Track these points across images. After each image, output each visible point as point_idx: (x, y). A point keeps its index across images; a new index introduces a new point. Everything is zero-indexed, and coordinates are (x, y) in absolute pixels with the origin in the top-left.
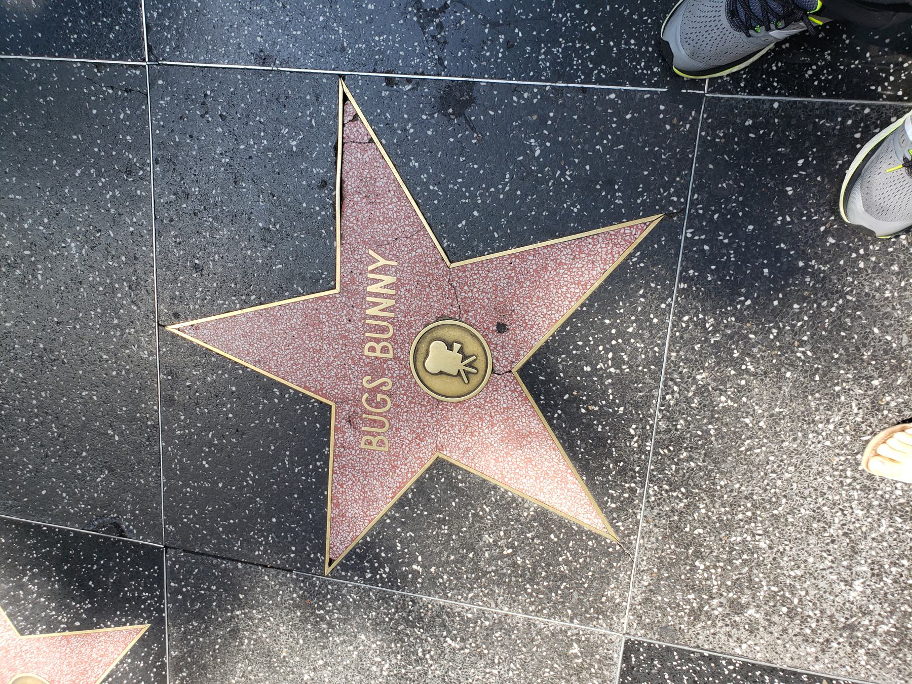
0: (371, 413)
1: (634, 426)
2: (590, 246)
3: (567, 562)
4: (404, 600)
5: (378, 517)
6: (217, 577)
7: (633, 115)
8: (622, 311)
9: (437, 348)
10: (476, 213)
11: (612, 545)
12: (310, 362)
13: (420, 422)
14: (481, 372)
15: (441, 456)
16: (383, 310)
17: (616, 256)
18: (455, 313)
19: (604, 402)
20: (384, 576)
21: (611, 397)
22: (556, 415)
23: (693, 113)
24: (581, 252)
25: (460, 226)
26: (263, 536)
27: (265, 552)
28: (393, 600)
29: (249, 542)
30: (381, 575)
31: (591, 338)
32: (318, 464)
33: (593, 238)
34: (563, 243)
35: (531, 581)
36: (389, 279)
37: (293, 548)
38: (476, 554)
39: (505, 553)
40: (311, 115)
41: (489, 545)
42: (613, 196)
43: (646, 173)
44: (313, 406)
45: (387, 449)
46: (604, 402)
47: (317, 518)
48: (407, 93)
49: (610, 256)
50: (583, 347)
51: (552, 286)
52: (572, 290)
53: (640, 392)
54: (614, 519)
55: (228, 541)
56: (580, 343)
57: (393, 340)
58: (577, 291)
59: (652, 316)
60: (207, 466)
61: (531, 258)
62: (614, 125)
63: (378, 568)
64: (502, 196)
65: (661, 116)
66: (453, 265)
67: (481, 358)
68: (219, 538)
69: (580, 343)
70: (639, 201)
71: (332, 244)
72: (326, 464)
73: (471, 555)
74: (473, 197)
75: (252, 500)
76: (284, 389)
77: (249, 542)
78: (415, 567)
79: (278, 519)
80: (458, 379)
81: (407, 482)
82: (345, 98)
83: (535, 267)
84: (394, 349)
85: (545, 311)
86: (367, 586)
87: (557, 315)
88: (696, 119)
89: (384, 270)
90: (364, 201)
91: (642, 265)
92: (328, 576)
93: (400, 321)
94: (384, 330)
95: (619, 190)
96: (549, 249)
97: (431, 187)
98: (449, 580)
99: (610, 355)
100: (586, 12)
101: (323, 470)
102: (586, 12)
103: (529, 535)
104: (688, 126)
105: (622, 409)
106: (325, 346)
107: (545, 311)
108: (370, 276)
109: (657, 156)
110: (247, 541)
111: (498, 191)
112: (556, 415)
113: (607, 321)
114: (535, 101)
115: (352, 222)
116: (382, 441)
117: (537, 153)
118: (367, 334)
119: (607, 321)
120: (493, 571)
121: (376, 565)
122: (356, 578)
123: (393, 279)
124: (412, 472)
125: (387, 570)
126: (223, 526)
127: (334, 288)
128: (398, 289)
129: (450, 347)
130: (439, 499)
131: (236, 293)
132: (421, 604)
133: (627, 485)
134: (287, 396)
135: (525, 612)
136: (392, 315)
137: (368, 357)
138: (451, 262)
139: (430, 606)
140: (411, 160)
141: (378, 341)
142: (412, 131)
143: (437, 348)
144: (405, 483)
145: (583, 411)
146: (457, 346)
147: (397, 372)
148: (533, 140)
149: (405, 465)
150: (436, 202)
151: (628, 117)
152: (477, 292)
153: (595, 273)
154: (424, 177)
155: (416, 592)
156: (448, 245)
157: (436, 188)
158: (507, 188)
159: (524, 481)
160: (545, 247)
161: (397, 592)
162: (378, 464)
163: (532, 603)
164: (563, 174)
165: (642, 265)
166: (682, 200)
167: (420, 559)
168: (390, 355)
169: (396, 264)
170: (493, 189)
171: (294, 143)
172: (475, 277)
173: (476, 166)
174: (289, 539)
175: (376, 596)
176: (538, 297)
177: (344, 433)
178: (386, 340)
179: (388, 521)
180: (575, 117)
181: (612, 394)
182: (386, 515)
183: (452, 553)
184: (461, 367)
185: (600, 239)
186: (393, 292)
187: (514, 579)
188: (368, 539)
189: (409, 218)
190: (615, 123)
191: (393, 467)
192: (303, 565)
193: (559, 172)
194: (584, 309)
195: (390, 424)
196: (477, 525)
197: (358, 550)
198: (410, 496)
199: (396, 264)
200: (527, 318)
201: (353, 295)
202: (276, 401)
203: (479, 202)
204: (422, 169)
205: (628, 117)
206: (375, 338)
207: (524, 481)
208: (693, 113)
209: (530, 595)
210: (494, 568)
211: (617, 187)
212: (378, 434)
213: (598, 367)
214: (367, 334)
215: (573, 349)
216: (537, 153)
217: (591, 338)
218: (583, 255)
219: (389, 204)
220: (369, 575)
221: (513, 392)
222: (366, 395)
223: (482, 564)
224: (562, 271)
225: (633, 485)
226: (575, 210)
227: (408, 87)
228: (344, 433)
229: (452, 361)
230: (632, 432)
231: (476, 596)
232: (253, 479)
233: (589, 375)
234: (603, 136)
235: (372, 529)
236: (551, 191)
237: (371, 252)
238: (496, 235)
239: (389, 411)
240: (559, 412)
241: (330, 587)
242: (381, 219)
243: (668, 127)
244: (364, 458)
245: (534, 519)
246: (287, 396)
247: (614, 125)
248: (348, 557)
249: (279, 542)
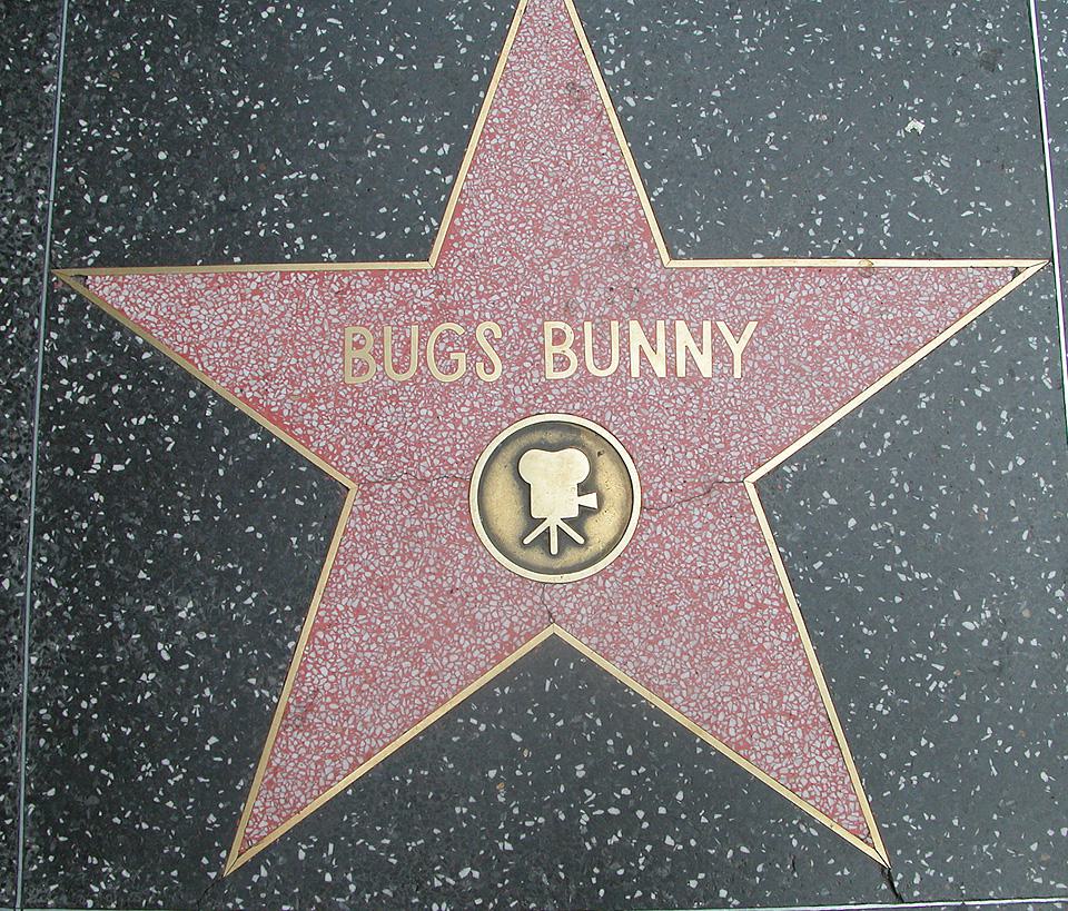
0: (423, 340)
1: (476, 874)
2: (818, 744)
3: (162, 774)
4: (19, 441)
5: (197, 372)
6: (16, 40)
7: (1046, 784)
8: (704, 820)
10: (852, 523)
11: (217, 863)
12: (514, 213)
13: (419, 444)
14: (558, 564)
15: (351, 496)
16: (688, 354)
17: (806, 794)
18: (657, 497)
19: (516, 811)
20: (68, 395)
21: (528, 824)
22: (474, 721)
23: (1061, 886)
24: (806, 729)
25: (826, 494)
26: (124, 134)
27: (88, 139)
28: (15, 417)
29: (104, 107)
30: (70, 387)
31: (642, 770)
32: (299, 241)
33: (832, 747)
34: (819, 694)
35: (107, 708)
36: (705, 365)
37: (104, 199)
38: (146, 586)
39: (160, 646)
40: (978, 209)
41: (172, 611)
42: (911, 771)
43: (956, 822)
44: (423, 224)
45: (350, 380)
46: (516, 811)
47: (178, 243)
48: (1039, 381)
49: (804, 782)
50: (623, 758)
51: (735, 683)
52: (732, 723)
53: (549, 877)
54: (273, 859)
55: (102, 62)
56: (630, 751)
57: (586, 378)
58: (732, 733)
59: (701, 876)
60: (265, 15)
61: (784, 637)
62: (1027, 754)
63: (83, 381)
64: (888, 568)
65: (1051, 833)
67: (586, 554)
68: (108, 42)
69: (630, 751)
70: (906, 818)
71: (758, 249)
72: (297, 259)
73: (142, 575)
74: (883, 514)
75: (201, 108)
76: (452, 164)
77: (104, 107)
78: (98, 458)
79: (167, 164)
81: (283, 428)
83: (767, 646)
84: (566, 381)
85: (687, 675)
86: (39, 360)
87: (679, 699)
88: (1052, 893)
89: (721, 353)
90: (846, 310)
91: (795, 843)
92: (50, 275)
93: (625, 396)
94: (603, 361)
95: (921, 778)
96: (804, 669)
97: (887, 435)
98: (81, 533)
99: (614, 811)
101: (286, 251)
103: (207, 692)
104: (1039, 880)
105: (508, 847)
106: (550, 242)
107: (687, 675)
108: (707, 326)
109: (986, 836)
110: (109, 102)
111: (896, 559)
112: (474, 721)
113: (680, 796)
114: (1053, 611)
115: (803, 288)
116: (365, 369)
117: (969, 625)
118: (588, 326)
119: (680, 796)
120: (115, 624)
121: (91, 376)
122: (54, 335)
123: (707, 373)
124: (306, 437)
125: (82, 400)
126: (135, 53)
127: (673, 256)
128: (687, 381)
129: (584, 489)
130: (256, 497)
131: (636, 69)
132: (16, 478)
133: (349, 877)
134: (437, 170)
135: (35, 700)
136: (635, 373)
137: (541, 328)
139: (14, 497)
140: (929, 395)
141: (578, 346)
142: (978, 393)
143: (575, 464)
144: (279, 423)
145: (492, 774)
146: (590, 500)
147: (517, 391)
148: (988, 614)
149: (320, 422)
150: (863, 446)
151: (1044, 776)
152: (706, 539)
153: (770, 759)
154: (903, 420)
155: (42, 464)
156: (787, 475)
157: (887, 444)
158: (903, 577)
159: (324, 671)
160: (806, 660)
161: (35, 424)
162: (314, 364)
163: (55, 711)
164: (938, 676)
165: (795, 843)
166: (916, 893)
167: (117, 468)
168: (551, 374)
169: (737, 375)
170: (898, 551)
171: (928, 179)
172: (733, 532)
173: (933, 515)
174: (124, 190)
175: (20, 379)
176: (709, 660)
177: (374, 291)
178: (583, 365)
179: (192, 394)
180: (1034, 685)
181: (537, 824)
182: (206, 388)
183: (139, 536)
184: (553, 522)
185: (832, 761)
186: (681, 372)
187: (104, 669)
188: (146, 356)
189: (827, 398)
190: (1032, 754)
191: (312, 396)
192: (68, 222)
193: (941, 668)
194: (699, 750)
195: (405, 383)
196: (212, 581)
197: (118, 335)
198: (253, 436)
199: (737, 375)
200: (667, 641)
201: (662, 292)
202: (424, 150)
203: (874, 528)
204: (918, 418)
205: (1044, 776)
206: (582, 341)
207: (324, 671)
208: (1061, 886)
209: (74, 707)
210: (122, 626)
211: (926, 775)
212: (380, 361)
213: (588, 792)
214: (588, 326)
215: (615, 739)
216: (969, 625)
217: (642, 770)
218: (799, 733)
219: (846, 357)
220: (64, 363)
221: (510, 631)
222: (459, 330)
223: (127, 599)
224: (766, 699)
225: (352, 888)
226: (879, 707)
227: (1047, 382)
228: (374, 291)
230: (464, 873)
231: (54, 594)
232: (248, 109)
233: (568, 774)
234: (1009, 738)
235: (170, 363)
236: (907, 658)
237: (752, 326)
238: (816, 566)
239: (431, 378)
240: (483, 727)
241: (26, 281)
242: (818, 343)
243: (1034, 847)
244: (323, 334)
245: (245, 699)
246: (437, 170)
247: (1027, 754)
248: (99, 315)
249: (114, 168)
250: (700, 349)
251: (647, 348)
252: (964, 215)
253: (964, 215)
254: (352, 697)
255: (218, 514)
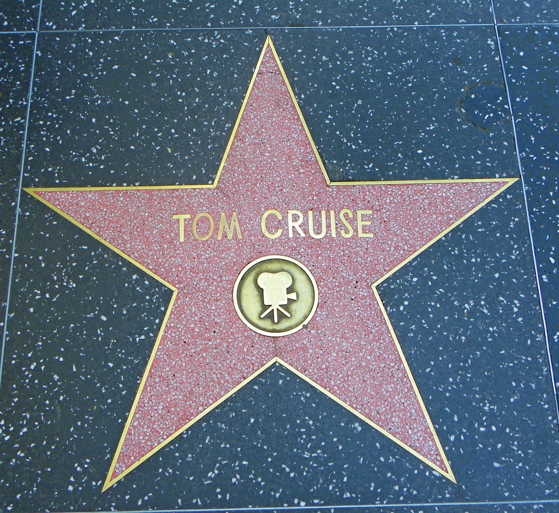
9: (284, 280)
14: (277, 327)
66: (333, 184)
80: (258, 308)
82: (38, 193)
100: (120, 100)
102: (120, 100)
126: (53, 172)
129: (290, 290)
138: (332, 181)
143: (284, 280)
146: (293, 296)
184: (275, 307)
229: (276, 298)
250: (35, 192)
251: (227, 227)
252: (74, 366)
253: (74, 366)
254: (164, 407)
255: (122, 307)
